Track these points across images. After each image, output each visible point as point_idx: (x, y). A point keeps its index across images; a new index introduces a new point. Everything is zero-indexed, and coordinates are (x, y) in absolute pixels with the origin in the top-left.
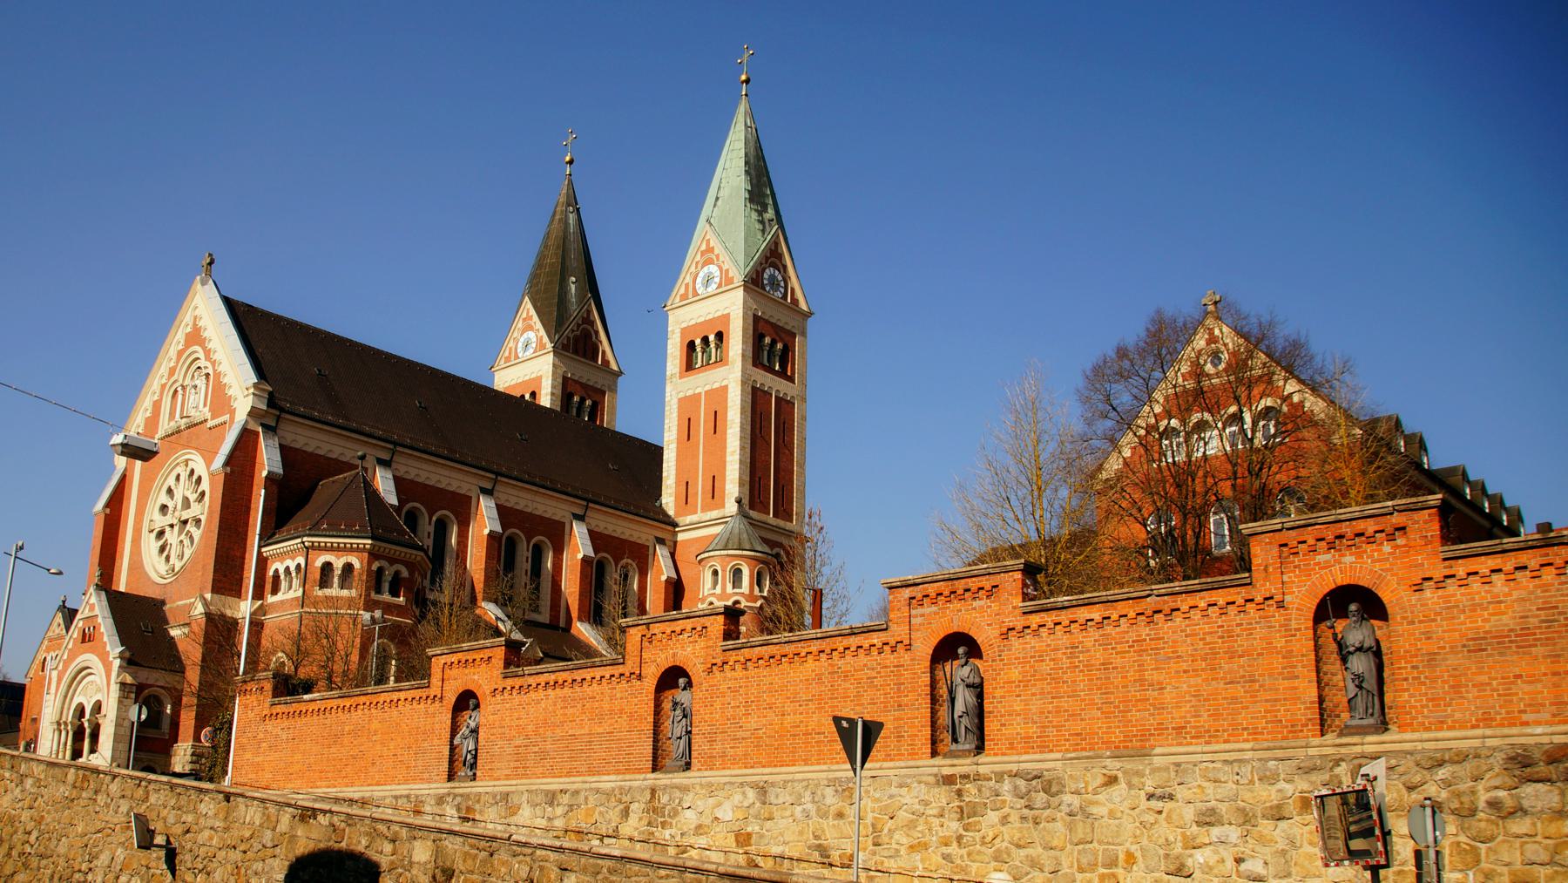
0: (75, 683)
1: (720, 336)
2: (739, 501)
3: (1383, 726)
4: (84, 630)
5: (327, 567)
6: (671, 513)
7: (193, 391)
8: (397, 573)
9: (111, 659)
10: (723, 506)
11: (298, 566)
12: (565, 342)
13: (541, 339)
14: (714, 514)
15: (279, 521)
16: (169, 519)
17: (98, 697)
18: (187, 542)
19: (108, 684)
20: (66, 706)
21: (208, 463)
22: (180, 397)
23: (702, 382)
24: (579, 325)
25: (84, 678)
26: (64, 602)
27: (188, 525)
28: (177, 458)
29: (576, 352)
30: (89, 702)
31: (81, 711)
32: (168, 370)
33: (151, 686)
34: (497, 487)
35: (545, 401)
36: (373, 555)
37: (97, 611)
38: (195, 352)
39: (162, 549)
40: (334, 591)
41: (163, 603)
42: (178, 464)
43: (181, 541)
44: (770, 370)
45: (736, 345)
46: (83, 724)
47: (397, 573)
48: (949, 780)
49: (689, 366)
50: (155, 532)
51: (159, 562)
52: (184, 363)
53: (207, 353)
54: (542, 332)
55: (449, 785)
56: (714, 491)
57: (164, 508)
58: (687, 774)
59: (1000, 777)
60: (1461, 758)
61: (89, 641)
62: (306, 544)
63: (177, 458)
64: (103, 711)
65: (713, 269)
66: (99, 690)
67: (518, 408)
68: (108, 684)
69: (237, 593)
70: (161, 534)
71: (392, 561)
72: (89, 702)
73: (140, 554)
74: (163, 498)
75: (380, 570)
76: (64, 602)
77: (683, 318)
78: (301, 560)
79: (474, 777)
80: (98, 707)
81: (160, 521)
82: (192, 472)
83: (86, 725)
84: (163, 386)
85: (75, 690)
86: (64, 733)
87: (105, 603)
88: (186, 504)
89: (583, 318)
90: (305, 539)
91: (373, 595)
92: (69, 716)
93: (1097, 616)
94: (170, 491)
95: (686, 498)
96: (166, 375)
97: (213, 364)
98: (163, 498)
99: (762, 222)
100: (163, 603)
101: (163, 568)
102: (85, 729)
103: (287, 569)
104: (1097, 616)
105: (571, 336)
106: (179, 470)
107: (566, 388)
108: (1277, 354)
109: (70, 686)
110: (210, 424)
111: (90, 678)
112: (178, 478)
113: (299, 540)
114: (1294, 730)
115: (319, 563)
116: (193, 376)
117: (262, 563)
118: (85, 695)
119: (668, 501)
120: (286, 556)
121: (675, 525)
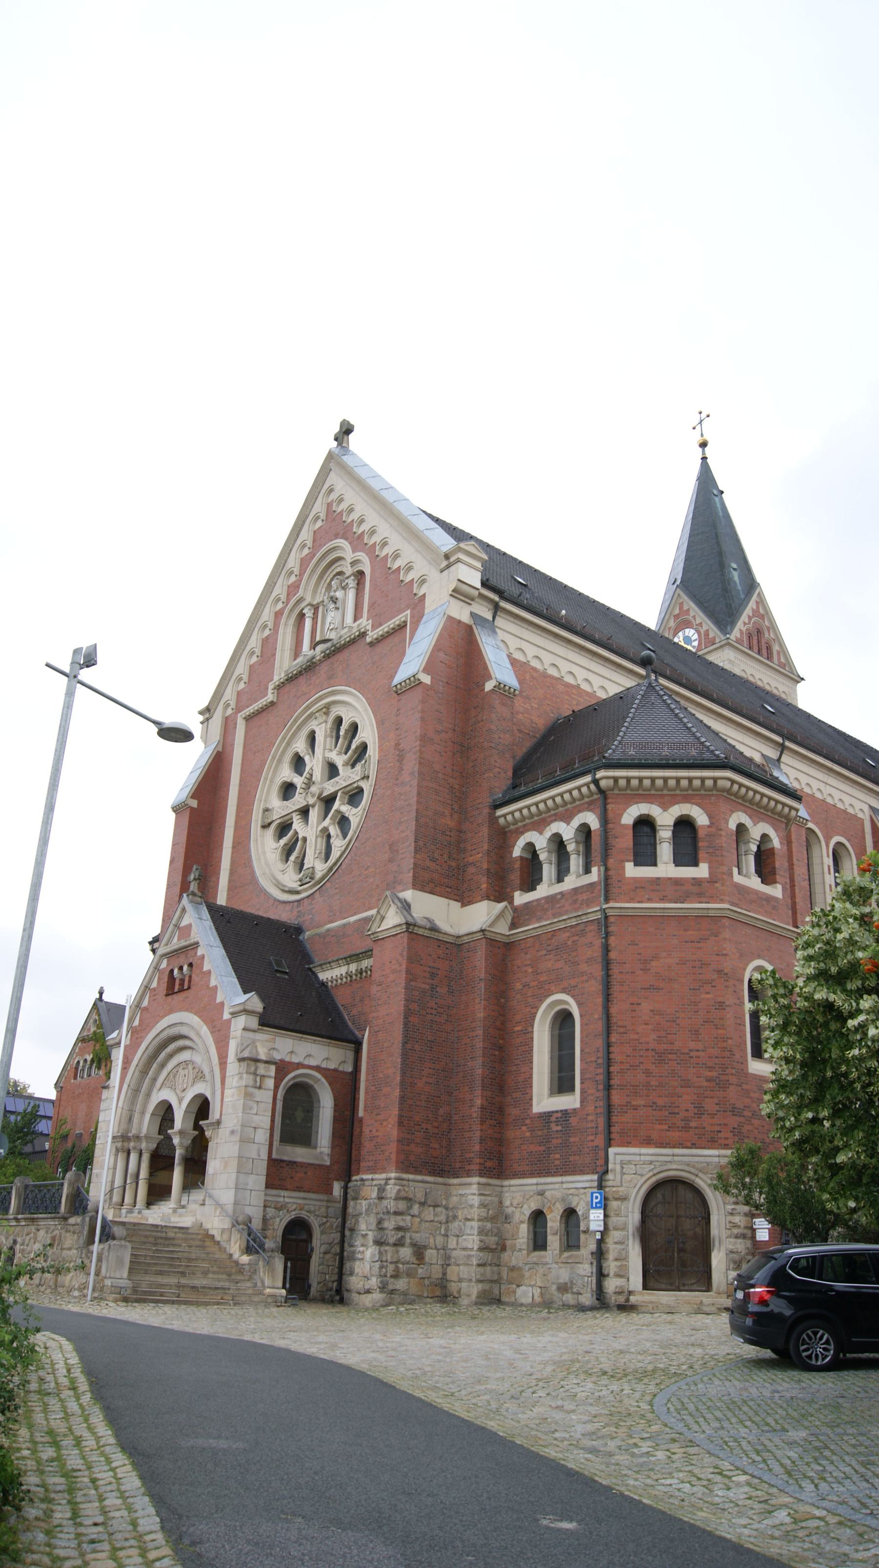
0: (163, 1055)
4: (172, 971)
5: (645, 824)
7: (332, 606)
8: (765, 837)
9: (226, 1016)
11: (585, 831)
12: (739, 636)
13: (707, 633)
16: (298, 800)
17: (200, 1088)
18: (334, 830)
19: (223, 1063)
20: (138, 1108)
22: (308, 623)
24: (750, 618)
25: (171, 1056)
26: (101, 993)
27: (337, 805)
28: (308, 707)
30: (180, 1101)
31: (166, 1113)
32: (285, 589)
33: (300, 1065)
34: (785, 758)
37: (195, 936)
38: (334, 549)
39: (288, 851)
41: (299, 930)
42: (312, 714)
43: (325, 830)
46: (169, 1138)
50: (273, 826)
51: (283, 871)
52: (313, 571)
53: (358, 542)
57: (288, 790)
61: (181, 990)
62: (603, 783)
63: (308, 707)
64: (214, 1114)
66: (200, 1076)
68: (223, 1063)
70: (284, 828)
72: (180, 1101)
73: (248, 863)
74: (287, 774)
76: (101, 993)
78: (592, 820)
80: (202, 1108)
81: (279, 808)
82: (339, 721)
83: (176, 1141)
84: (278, 615)
85: (155, 1080)
86: (133, 1157)
87: (209, 923)
88: (332, 770)
89: (753, 610)
90: (600, 774)
92: (145, 1124)
94: (298, 763)
96: (283, 597)
97: (371, 551)
98: (287, 774)
100: (299, 930)
101: (291, 879)
102: (174, 1149)
103: (558, 843)
105: (744, 629)
106: (313, 725)
108: (375, 1015)
109: (144, 1072)
110: (371, 636)
111: (185, 1056)
112: (312, 738)
113: (588, 778)
116: (330, 585)
118: (173, 1088)
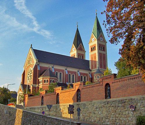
1: (95, 47)
2: (98, 67)
3: (110, 98)
6: (91, 69)
8: (53, 80)
10: (96, 68)
14: (95, 69)
15: (40, 75)
21: (32, 68)
23: (93, 52)
29: (79, 50)
35: (76, 57)
36: (50, 79)
40: (46, 83)
44: (102, 50)
45: (97, 48)
47: (53, 80)
48: (78, 104)
49: (92, 51)
54: (75, 48)
55: (106, 100)
56: (95, 67)
58: (110, 99)
59: (81, 104)
60: (115, 101)
65: (93, 38)
67: (72, 58)
69: (36, 84)
71: (52, 79)
75: (51, 80)
77: (91, 44)
79: (80, 101)
91: (50, 83)
93: (88, 87)
94: (29, 72)
95: (92, 68)
99: (99, 32)
104: (88, 87)
107: (79, 55)
114: (103, 99)
115: (44, 80)
117: (39, 80)
119: (90, 68)
120: (41, 79)
121: (91, 71)
